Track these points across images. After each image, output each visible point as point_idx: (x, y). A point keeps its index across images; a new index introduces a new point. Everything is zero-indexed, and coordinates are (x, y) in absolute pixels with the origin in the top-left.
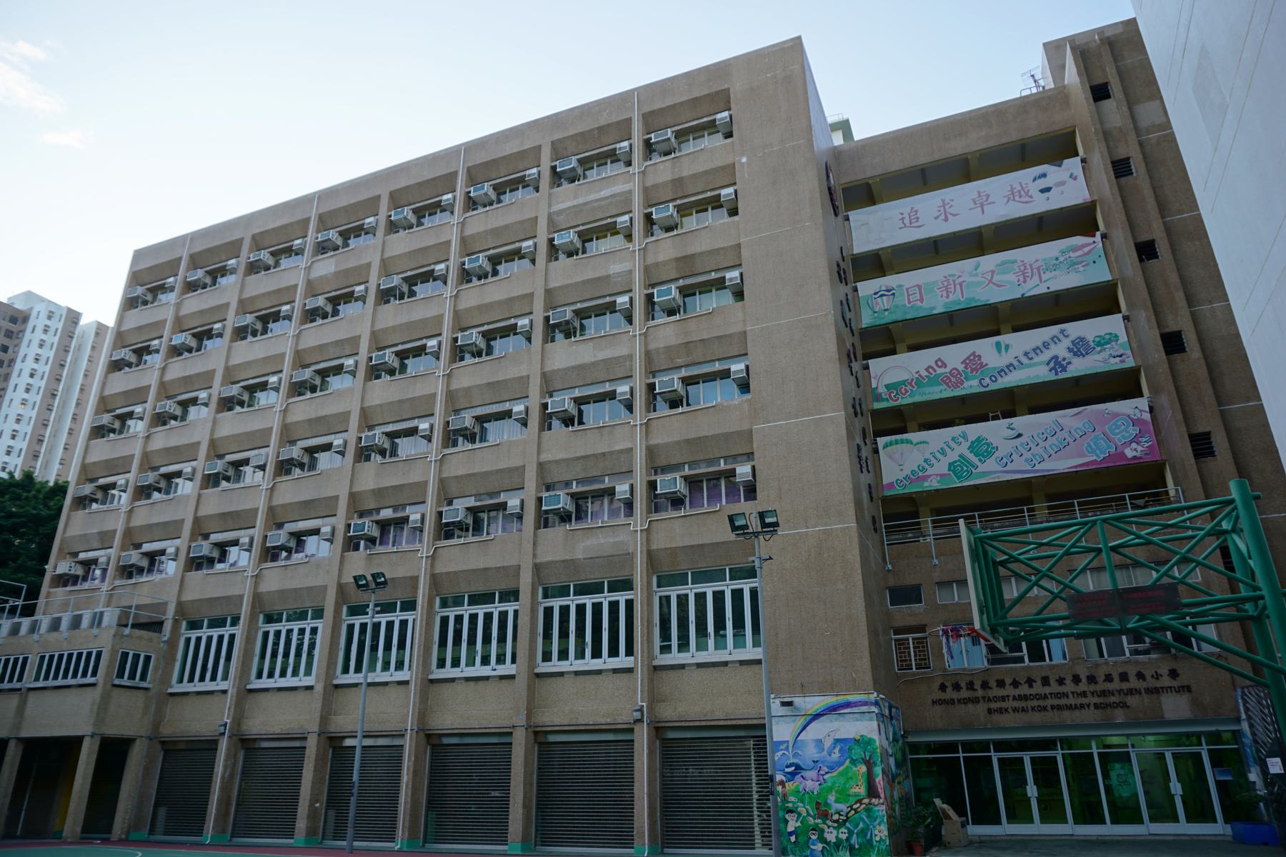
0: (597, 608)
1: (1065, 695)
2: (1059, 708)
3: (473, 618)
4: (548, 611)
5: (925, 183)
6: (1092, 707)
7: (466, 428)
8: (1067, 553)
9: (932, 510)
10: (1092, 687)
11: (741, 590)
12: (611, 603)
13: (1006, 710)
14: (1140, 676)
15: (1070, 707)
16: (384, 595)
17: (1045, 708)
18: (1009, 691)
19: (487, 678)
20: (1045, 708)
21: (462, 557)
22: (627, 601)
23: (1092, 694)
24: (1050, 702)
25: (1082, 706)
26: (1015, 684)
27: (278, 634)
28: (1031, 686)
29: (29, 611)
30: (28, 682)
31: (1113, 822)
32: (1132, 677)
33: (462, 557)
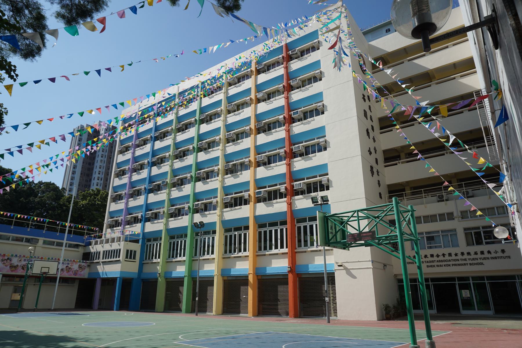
0: (265, 232)
1: (458, 260)
2: (455, 265)
3: (271, 232)
4: (299, 228)
5: (407, 53)
6: (469, 265)
7: (230, 168)
8: (385, 215)
9: (457, 180)
10: (469, 257)
11: (300, 227)
12: (270, 231)
13: (434, 266)
14: (489, 252)
15: (459, 265)
16: (203, 230)
17: (449, 265)
18: (435, 258)
19: (277, 254)
20: (449, 265)
21: (232, 214)
22: (304, 226)
23: (480, 259)
24: (436, 264)
25: (465, 264)
26: (438, 256)
27: (150, 245)
28: (444, 256)
29: (100, 237)
30: (101, 260)
31: (478, 310)
32: (486, 253)
33: (232, 214)
